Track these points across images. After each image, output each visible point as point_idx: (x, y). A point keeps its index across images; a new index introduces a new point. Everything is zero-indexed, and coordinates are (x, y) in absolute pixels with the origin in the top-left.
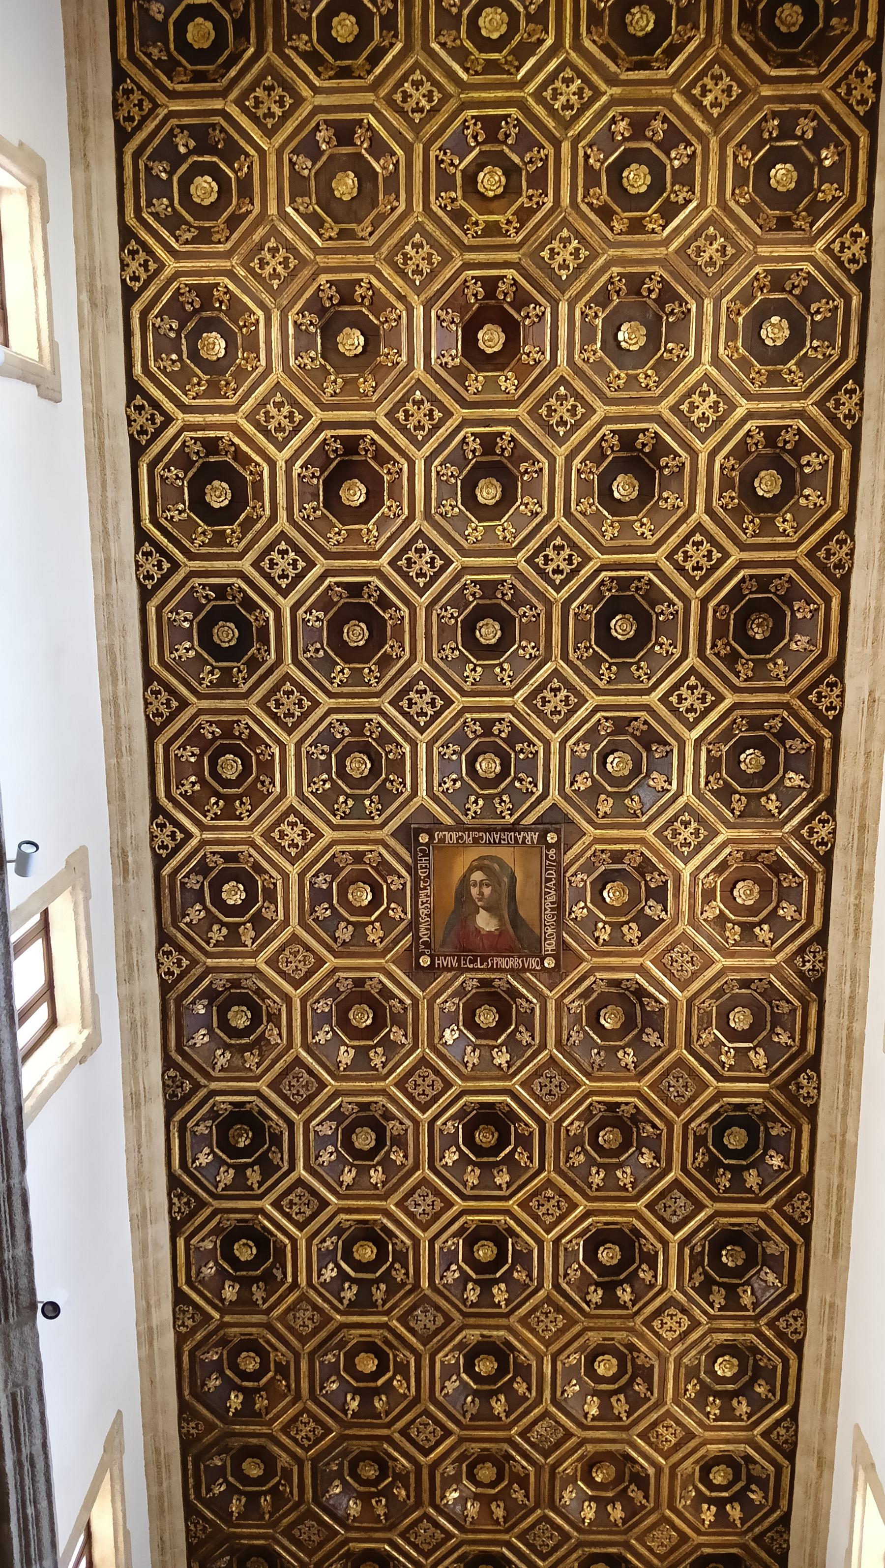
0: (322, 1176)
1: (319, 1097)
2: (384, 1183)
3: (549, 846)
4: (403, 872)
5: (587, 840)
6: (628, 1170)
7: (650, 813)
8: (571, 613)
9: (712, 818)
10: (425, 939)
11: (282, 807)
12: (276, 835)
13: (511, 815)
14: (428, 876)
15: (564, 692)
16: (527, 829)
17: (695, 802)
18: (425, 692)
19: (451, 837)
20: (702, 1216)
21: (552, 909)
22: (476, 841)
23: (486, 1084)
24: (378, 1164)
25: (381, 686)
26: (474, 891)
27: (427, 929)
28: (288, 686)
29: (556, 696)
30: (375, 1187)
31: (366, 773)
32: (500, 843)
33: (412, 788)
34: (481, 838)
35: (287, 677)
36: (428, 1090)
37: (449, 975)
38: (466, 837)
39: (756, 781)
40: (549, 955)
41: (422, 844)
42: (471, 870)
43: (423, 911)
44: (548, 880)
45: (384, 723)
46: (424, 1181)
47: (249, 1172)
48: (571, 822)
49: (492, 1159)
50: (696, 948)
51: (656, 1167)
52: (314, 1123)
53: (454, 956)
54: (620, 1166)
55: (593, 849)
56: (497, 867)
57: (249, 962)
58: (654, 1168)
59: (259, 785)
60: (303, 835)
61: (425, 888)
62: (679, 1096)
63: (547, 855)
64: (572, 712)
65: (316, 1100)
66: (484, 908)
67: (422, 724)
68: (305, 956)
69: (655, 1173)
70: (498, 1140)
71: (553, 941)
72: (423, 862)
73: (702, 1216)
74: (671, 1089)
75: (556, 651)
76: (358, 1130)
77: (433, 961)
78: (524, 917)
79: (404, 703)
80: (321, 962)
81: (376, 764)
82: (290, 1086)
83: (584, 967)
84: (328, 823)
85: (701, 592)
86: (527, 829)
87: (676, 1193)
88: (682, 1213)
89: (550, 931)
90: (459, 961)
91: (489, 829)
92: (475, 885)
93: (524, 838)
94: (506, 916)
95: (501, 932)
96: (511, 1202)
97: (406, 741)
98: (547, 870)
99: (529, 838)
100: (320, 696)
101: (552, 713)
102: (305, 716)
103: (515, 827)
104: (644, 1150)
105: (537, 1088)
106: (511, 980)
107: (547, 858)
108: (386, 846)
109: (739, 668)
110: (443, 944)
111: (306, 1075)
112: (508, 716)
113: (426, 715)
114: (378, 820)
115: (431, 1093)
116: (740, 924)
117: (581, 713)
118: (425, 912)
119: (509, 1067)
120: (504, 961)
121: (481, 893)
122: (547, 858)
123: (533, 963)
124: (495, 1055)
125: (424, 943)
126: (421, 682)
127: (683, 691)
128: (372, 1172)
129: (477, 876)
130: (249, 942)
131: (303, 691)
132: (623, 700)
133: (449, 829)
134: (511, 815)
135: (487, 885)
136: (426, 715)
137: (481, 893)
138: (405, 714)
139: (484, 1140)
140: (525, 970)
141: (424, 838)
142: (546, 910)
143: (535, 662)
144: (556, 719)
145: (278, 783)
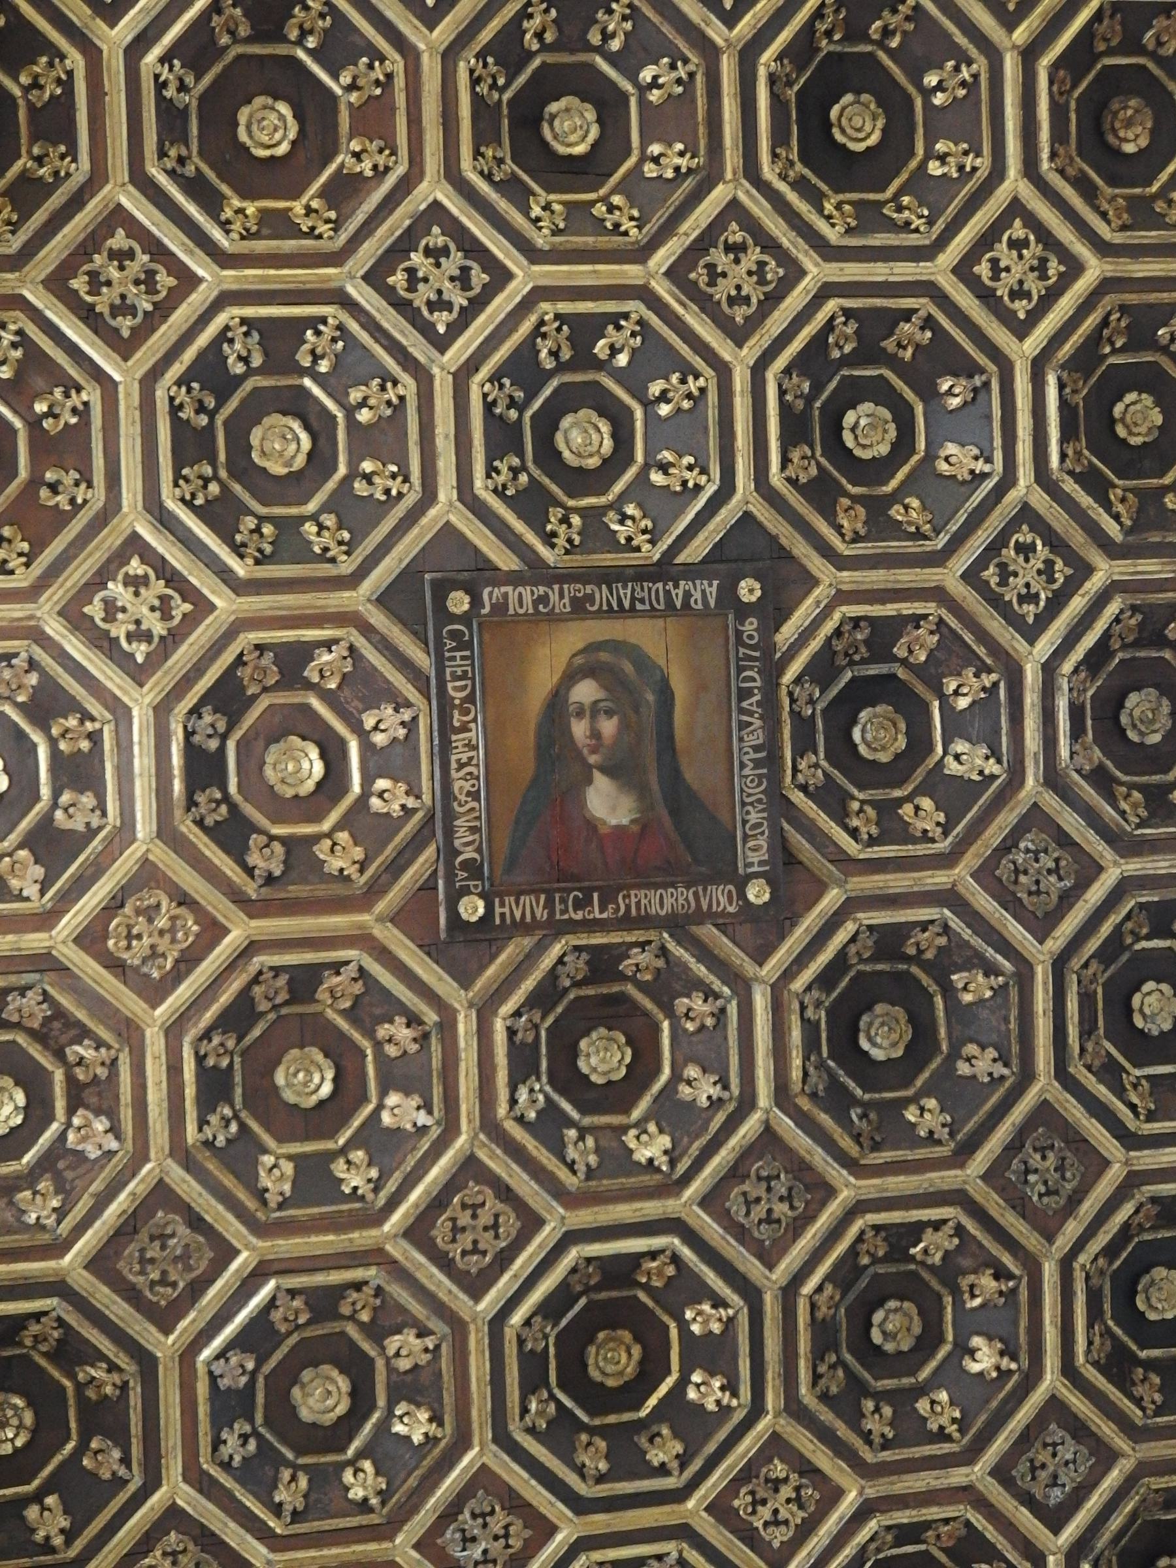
0: (229, 1494)
1: (219, 1284)
2: (384, 1496)
3: (743, 611)
4: (410, 692)
5: (820, 593)
6: (943, 1396)
7: (953, 527)
8: (762, 72)
9: (1077, 538)
10: (469, 854)
11: (110, 539)
12: (95, 610)
13: (652, 542)
14: (471, 699)
15: (754, 254)
16: (691, 572)
17: (1041, 501)
18: (445, 251)
19: (520, 599)
20: (1113, 1478)
21: (757, 764)
22: (579, 607)
23: (624, 1212)
24: (361, 1454)
25: (343, 237)
26: (579, 729)
27: (474, 830)
28: (119, 240)
29: (737, 261)
30: (363, 1506)
31: (300, 462)
32: (633, 608)
33: (424, 485)
34: (590, 598)
35: (118, 217)
36: (486, 1241)
37: (527, 942)
38: (554, 597)
39: (1147, 463)
40: (756, 875)
41: (454, 618)
42: (571, 677)
43: (460, 786)
44: (744, 694)
45: (354, 326)
46: (483, 1477)
47: (32, 1513)
48: (786, 556)
49: (627, 1417)
50: (1064, 840)
51: (1010, 1372)
52: (206, 1353)
53: (536, 892)
54: (921, 1390)
55: (837, 616)
56: (628, 668)
57: (35, 941)
58: (1004, 1374)
59: (44, 493)
60: (163, 608)
61: (464, 728)
62: (1049, 1193)
63: (739, 634)
64: (772, 300)
65: (212, 1292)
66: (604, 770)
67: (441, 329)
68: (173, 919)
69: (1009, 1386)
70: (641, 1363)
71: (763, 842)
72: (457, 663)
73: (1113, 1478)
74: (1032, 1178)
75: (732, 158)
76: (307, 1375)
77: (489, 908)
78: (695, 785)
79: (398, 279)
80: (214, 931)
81: (322, 441)
82: (143, 1261)
83: (832, 899)
84: (224, 574)
85: (1021, 34)
86: (691, 572)
87: (1055, 1432)
88: (1069, 1479)
89: (754, 817)
90: (550, 904)
91: (608, 577)
92: (580, 714)
93: (687, 595)
94: (655, 787)
95: (645, 827)
96: (691, 1504)
97: (405, 369)
98: (740, 670)
99: (697, 595)
100: (199, 265)
101: (731, 301)
102: (162, 311)
103: (664, 570)
104: (977, 1341)
105: (737, 1209)
106: (671, 945)
107: (739, 641)
108: (367, 629)
109: (795, 455)
110: (512, 863)
111: (183, 1230)
112: (635, 307)
113: (448, 306)
114: (347, 566)
115: (492, 1245)
116: (1141, 788)
117: (795, 301)
118: (467, 786)
119: (672, 1163)
120: (654, 896)
121: (596, 734)
122: (739, 641)
123: (720, 897)
124: (632, 1145)
125: (465, 865)
126: (436, 230)
127: (1002, 250)
128: (348, 1476)
129: (585, 692)
130: (32, 891)
131: (158, 251)
132: (878, 272)
133: (515, 579)
134: (652, 542)
135: (609, 713)
136: (448, 306)
137: (596, 734)
138: (402, 306)
139: (610, 1369)
140: (700, 917)
141: (459, 602)
142: (742, 766)
143: (689, 184)
144: (740, 314)
145: (99, 478)
